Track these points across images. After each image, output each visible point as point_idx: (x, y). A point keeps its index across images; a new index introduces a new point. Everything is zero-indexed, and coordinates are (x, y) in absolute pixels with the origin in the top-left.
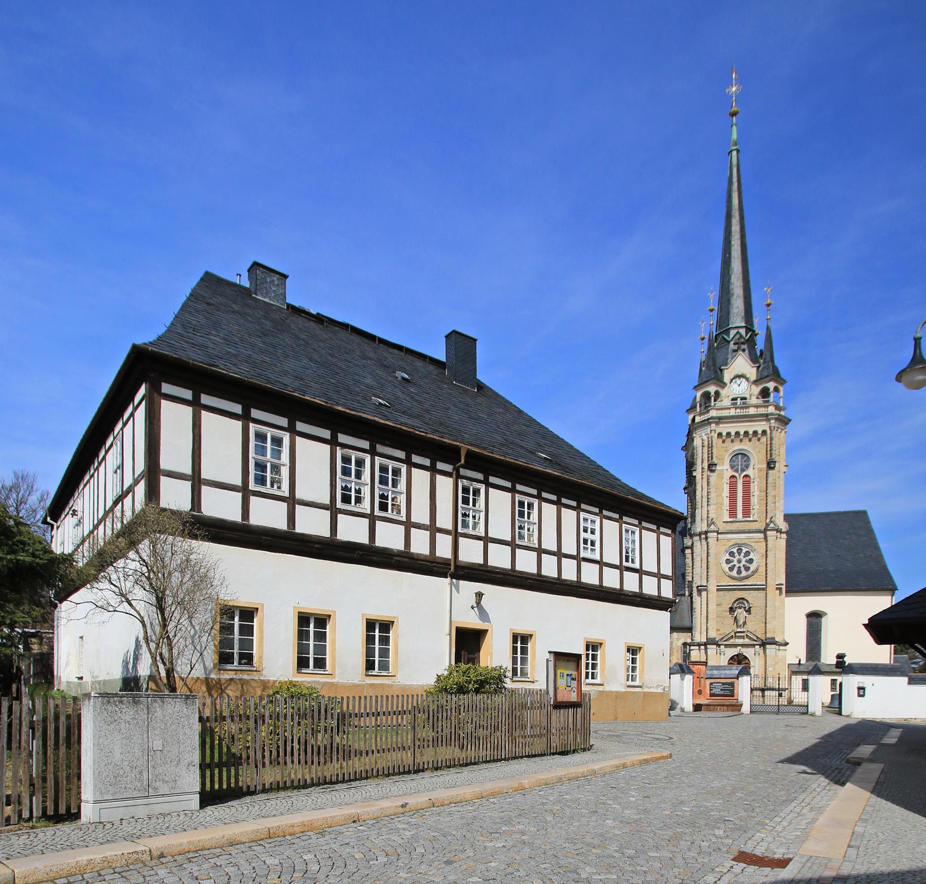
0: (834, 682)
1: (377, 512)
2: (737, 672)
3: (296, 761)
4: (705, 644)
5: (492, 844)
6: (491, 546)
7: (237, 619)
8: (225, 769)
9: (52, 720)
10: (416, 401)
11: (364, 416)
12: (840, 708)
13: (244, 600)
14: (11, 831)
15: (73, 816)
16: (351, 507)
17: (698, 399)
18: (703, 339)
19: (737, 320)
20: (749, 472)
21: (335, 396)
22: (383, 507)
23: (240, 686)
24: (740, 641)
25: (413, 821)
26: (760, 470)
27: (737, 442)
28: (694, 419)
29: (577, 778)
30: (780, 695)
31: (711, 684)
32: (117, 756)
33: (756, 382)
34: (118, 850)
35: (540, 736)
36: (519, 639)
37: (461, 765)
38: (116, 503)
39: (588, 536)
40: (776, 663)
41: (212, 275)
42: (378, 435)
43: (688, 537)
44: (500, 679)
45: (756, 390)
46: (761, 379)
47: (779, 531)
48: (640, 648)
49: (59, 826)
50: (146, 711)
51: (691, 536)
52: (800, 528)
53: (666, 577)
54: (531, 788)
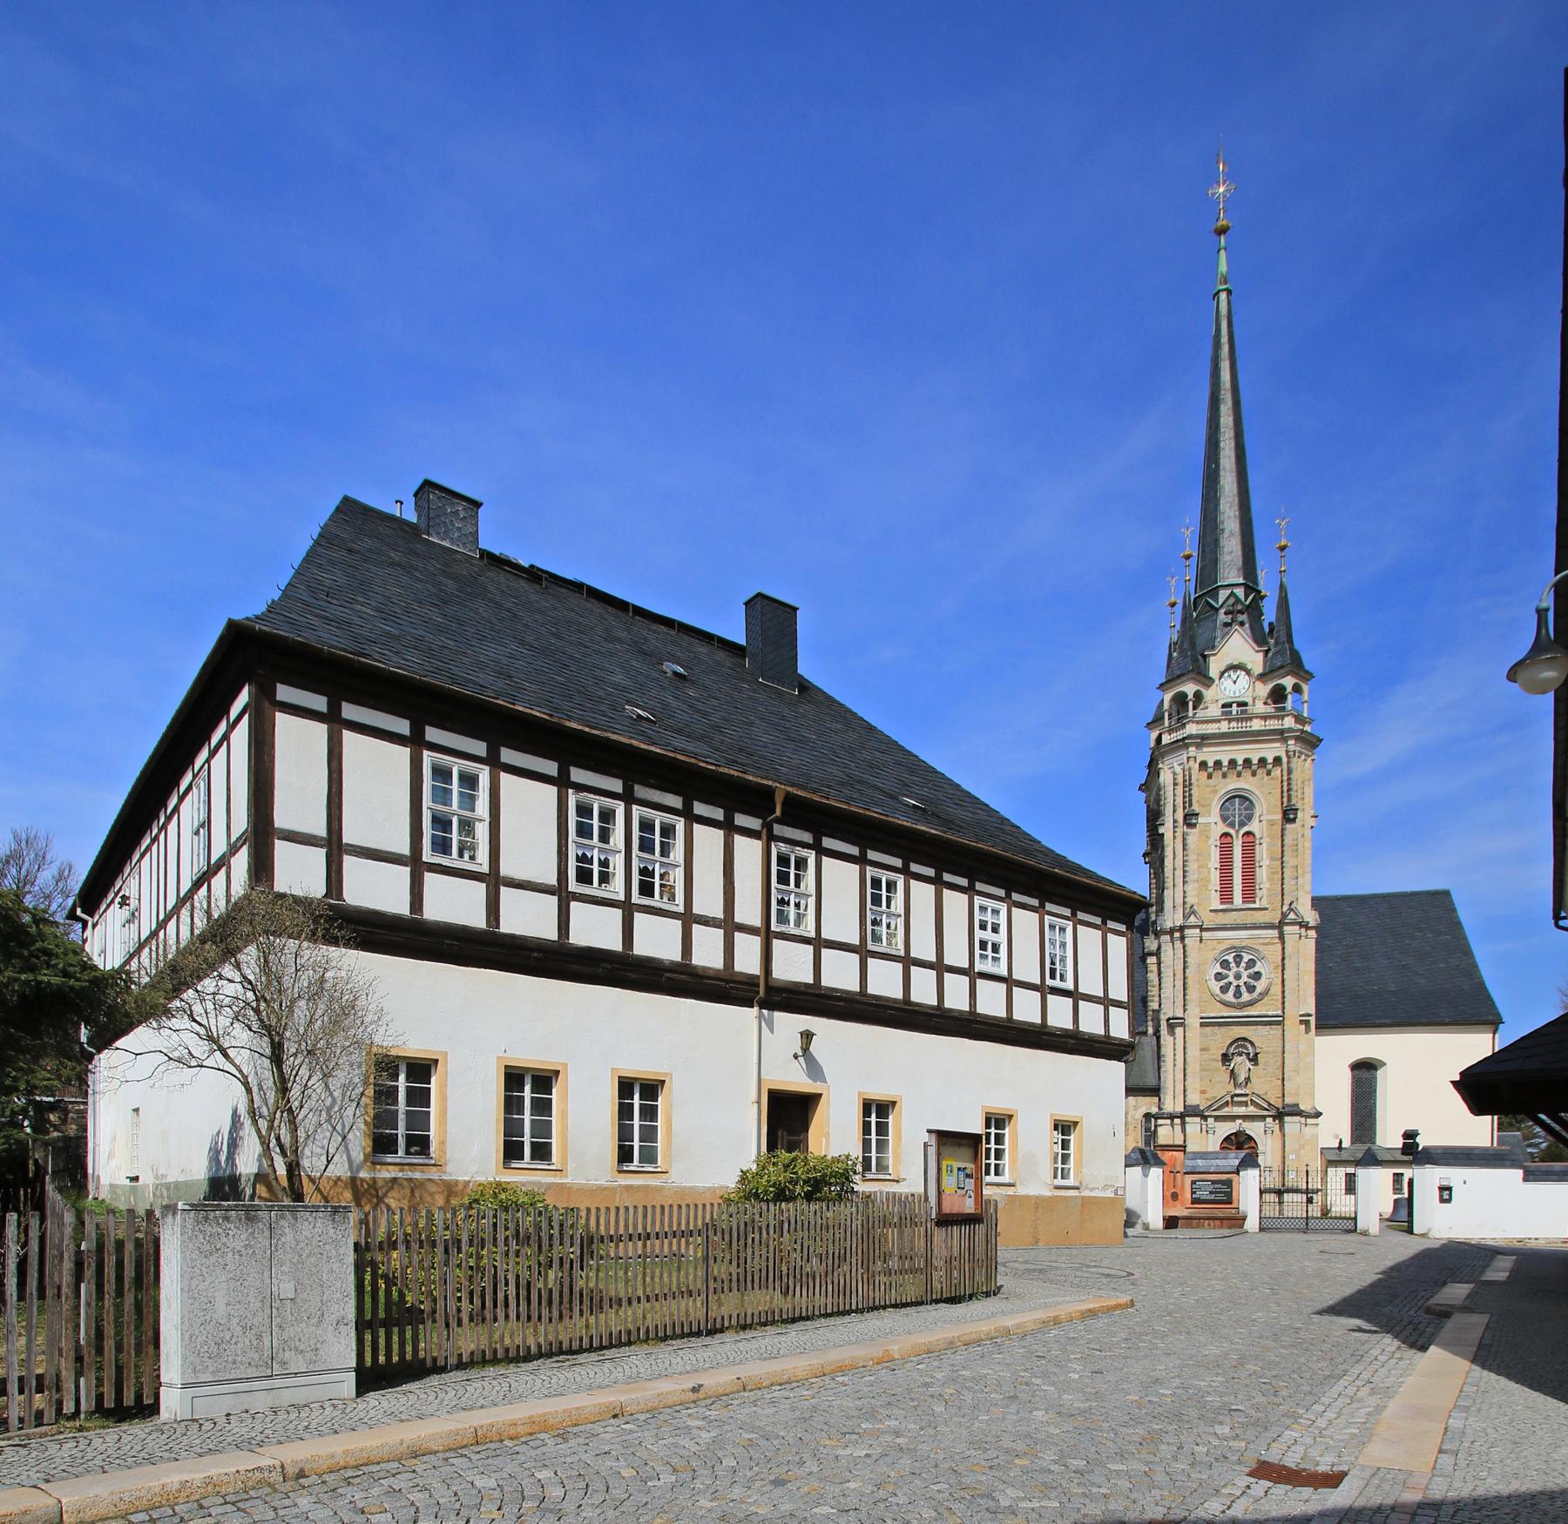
0: (1398, 1178)
1: (636, 898)
2: (1237, 1162)
3: (513, 1315)
4: (1182, 1116)
5: (848, 1452)
6: (826, 953)
7: (402, 1077)
8: (396, 1330)
9: (112, 1249)
10: (699, 711)
11: (614, 737)
12: (1410, 1222)
13: (415, 1046)
14: (46, 1435)
15: (147, 1409)
16: (593, 890)
17: (1166, 706)
18: (1173, 605)
19: (1230, 573)
20: (1254, 826)
21: (565, 705)
22: (646, 889)
23: (408, 1192)
24: (1241, 1110)
26: (1271, 823)
27: (1232, 777)
29: (978, 1342)
30: (1310, 1201)
31: (1193, 1182)
32: (221, 1307)
33: (1262, 677)
34: (229, 1466)
35: (913, 1271)
36: (874, 1109)
37: (784, 1321)
38: (197, 885)
39: (988, 935)
40: (1302, 1147)
41: (355, 502)
42: (637, 769)
43: (1152, 936)
44: (845, 1177)
45: (1263, 690)
47: (1304, 925)
48: (1076, 1123)
49: (125, 1426)
50: (267, 1233)
51: (1157, 935)
52: (1341, 921)
53: (1118, 1004)
54: (904, 1360)
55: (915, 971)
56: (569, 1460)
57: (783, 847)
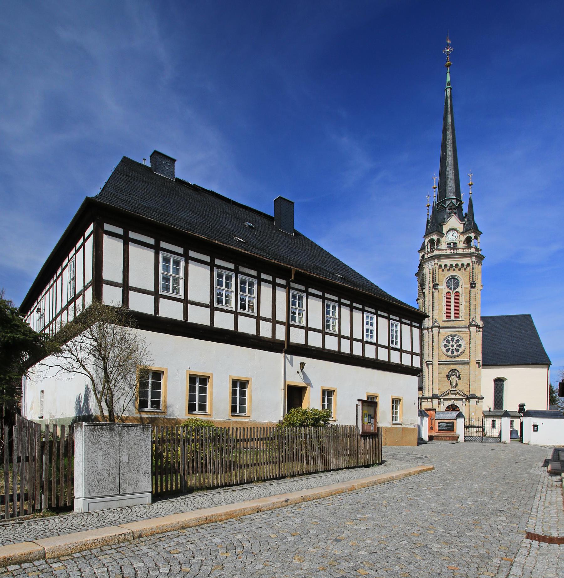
2: (456, 416)
3: (208, 470)
4: (431, 398)
10: (259, 240)
11: (232, 247)
13: (156, 366)
15: (70, 508)
16: (223, 307)
22: (243, 307)
24: (454, 396)
25: (296, 511)
26: (466, 288)
28: (423, 256)
31: (439, 423)
32: (100, 466)
33: (462, 233)
38: (69, 303)
41: (128, 159)
42: (240, 260)
45: (463, 238)
46: (466, 231)
47: (478, 327)
48: (400, 400)
55: (342, 340)
56: (247, 530)
57: (295, 292)
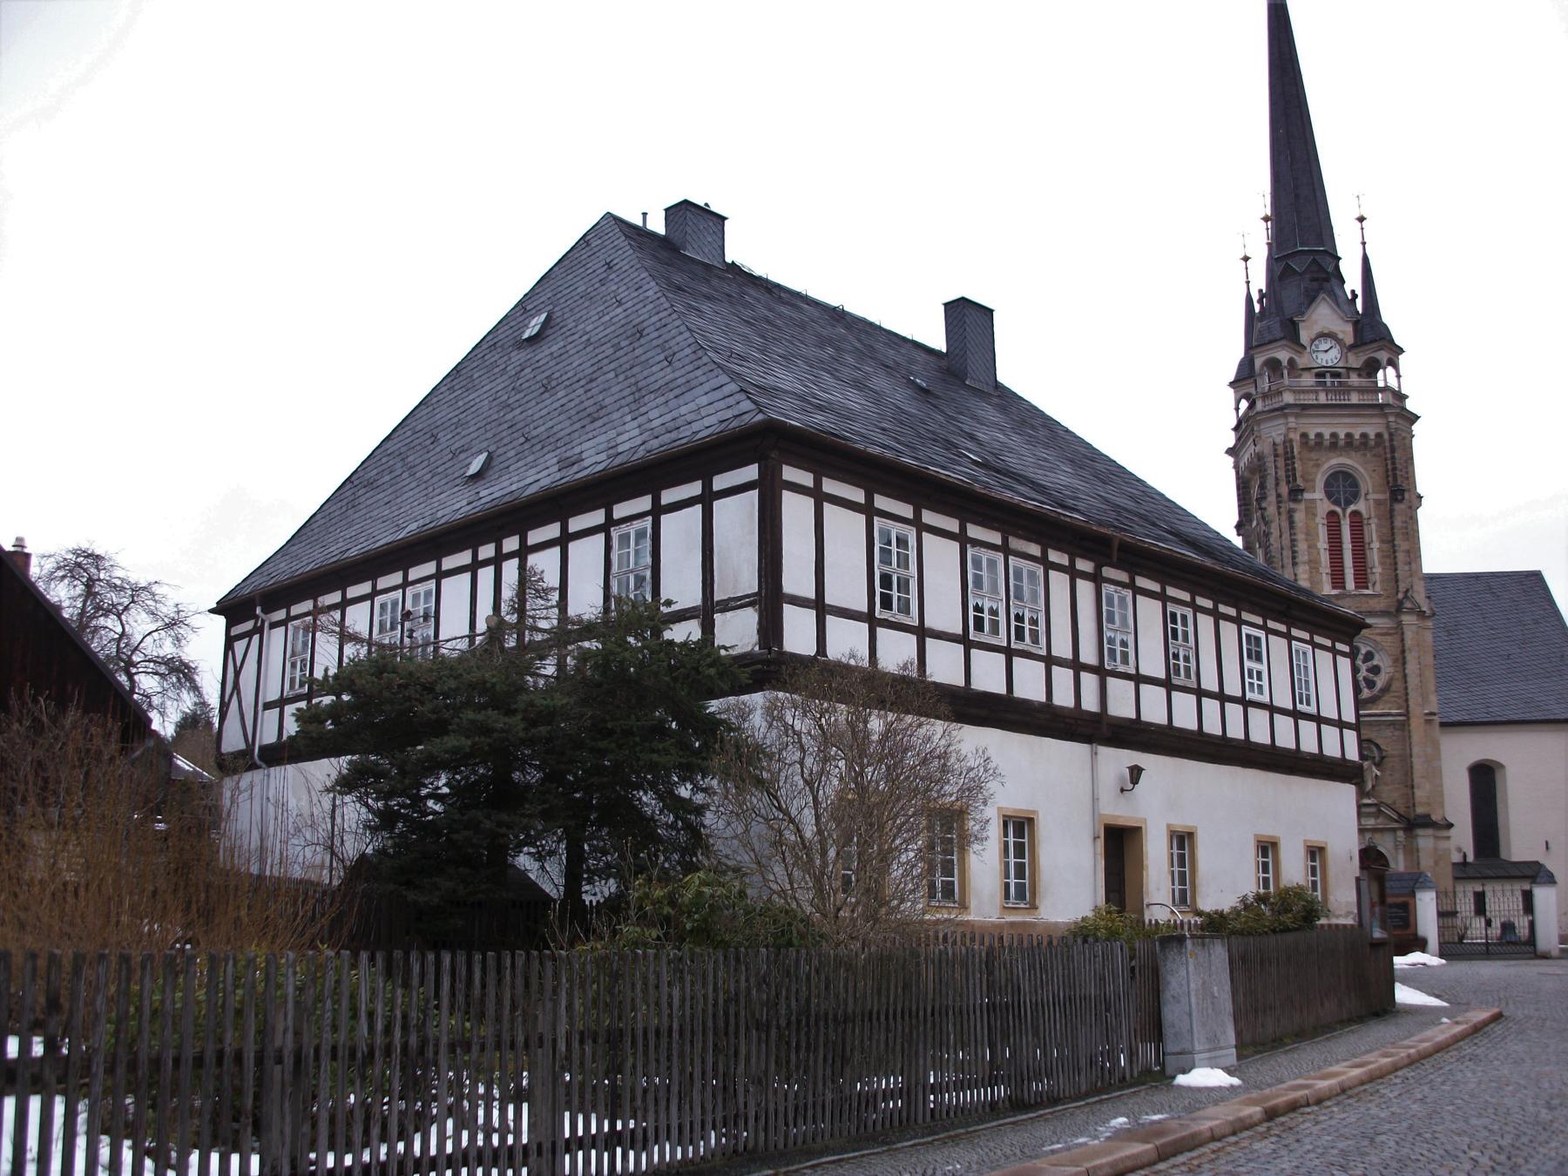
20: (1360, 506)
26: (1378, 503)
